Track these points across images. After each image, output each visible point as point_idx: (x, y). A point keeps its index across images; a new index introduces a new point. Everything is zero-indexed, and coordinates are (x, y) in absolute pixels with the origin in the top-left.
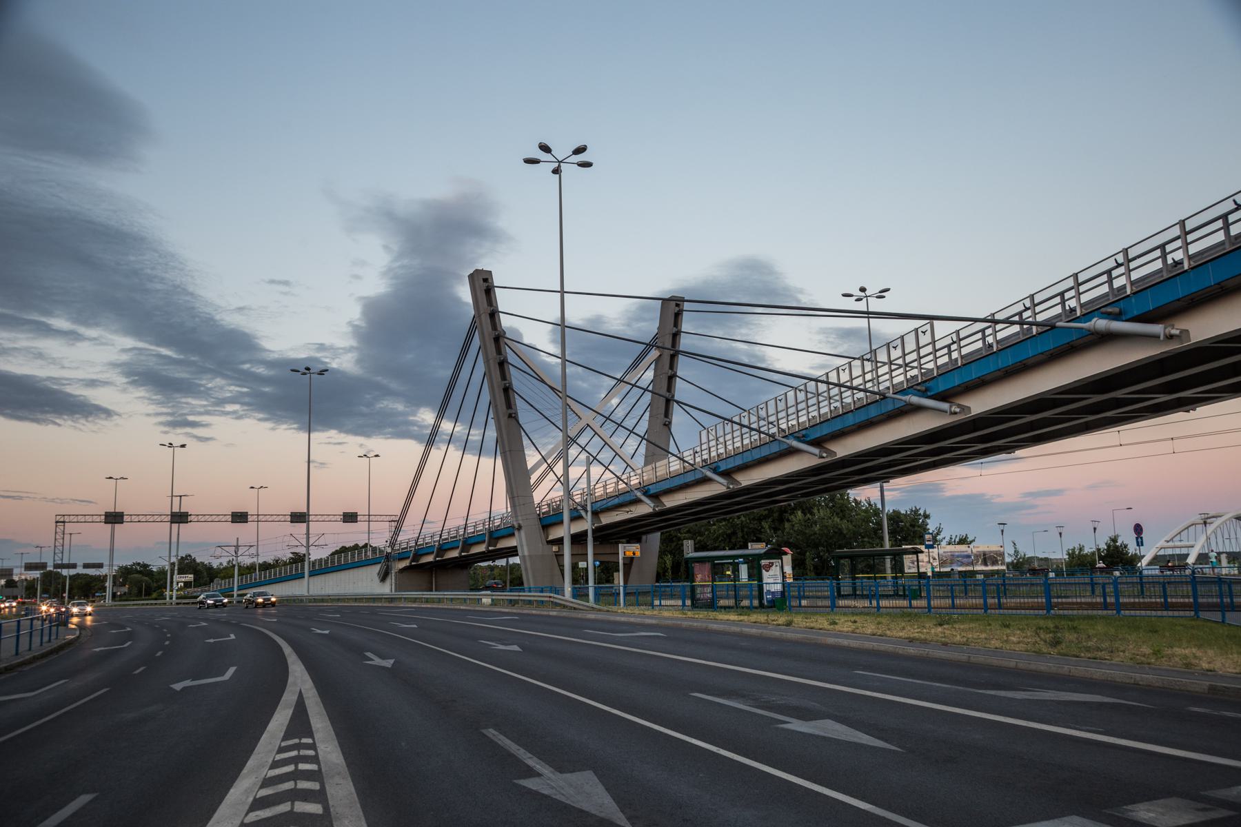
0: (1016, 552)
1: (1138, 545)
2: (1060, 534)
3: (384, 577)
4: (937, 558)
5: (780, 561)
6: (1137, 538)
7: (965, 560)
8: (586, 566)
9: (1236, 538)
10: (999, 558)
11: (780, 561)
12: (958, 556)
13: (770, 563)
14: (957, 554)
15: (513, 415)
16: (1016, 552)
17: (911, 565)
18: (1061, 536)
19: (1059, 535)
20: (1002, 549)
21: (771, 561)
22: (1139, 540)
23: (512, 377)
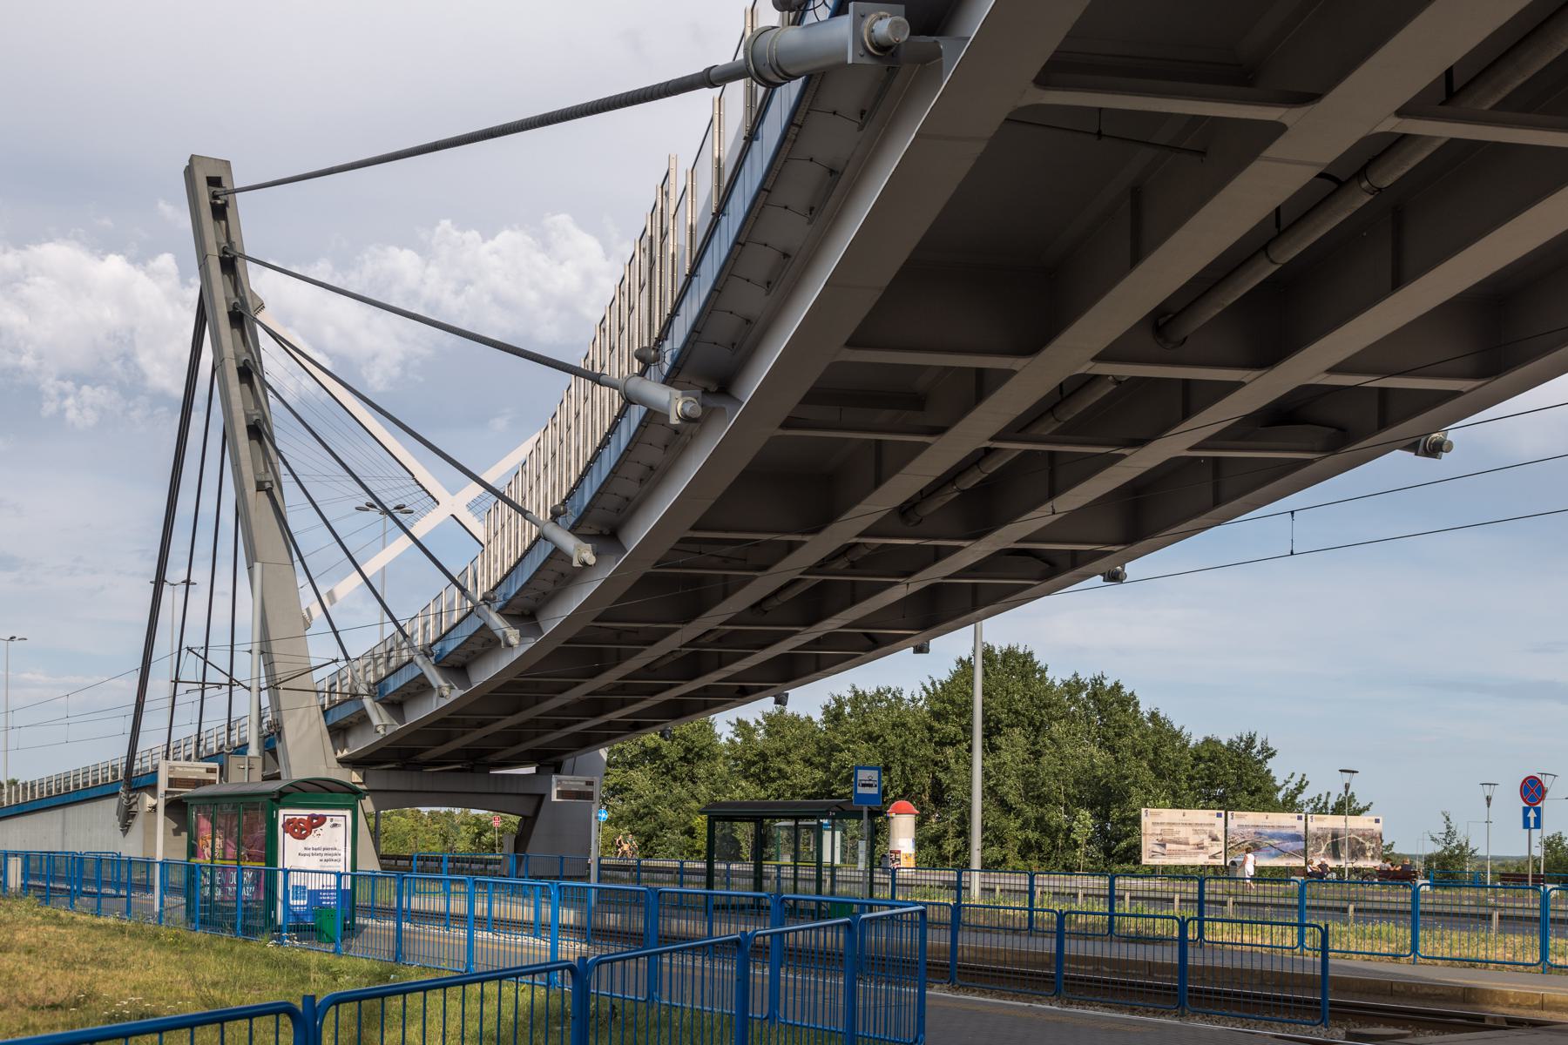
0: (1450, 833)
1: (1526, 825)
2: (1489, 799)
3: (127, 818)
4: (1221, 836)
5: (348, 813)
6: (1526, 811)
7: (1290, 845)
8: (1303, 847)
9: (188, 582)
10: (1368, 845)
11: (348, 813)
12: (1272, 837)
13: (312, 817)
14: (1269, 831)
15: (268, 485)
16: (1450, 833)
17: (1158, 849)
18: (1489, 805)
19: (1486, 802)
20: (589, 789)
21: (318, 812)
22: (1532, 814)
23: (603, 479)
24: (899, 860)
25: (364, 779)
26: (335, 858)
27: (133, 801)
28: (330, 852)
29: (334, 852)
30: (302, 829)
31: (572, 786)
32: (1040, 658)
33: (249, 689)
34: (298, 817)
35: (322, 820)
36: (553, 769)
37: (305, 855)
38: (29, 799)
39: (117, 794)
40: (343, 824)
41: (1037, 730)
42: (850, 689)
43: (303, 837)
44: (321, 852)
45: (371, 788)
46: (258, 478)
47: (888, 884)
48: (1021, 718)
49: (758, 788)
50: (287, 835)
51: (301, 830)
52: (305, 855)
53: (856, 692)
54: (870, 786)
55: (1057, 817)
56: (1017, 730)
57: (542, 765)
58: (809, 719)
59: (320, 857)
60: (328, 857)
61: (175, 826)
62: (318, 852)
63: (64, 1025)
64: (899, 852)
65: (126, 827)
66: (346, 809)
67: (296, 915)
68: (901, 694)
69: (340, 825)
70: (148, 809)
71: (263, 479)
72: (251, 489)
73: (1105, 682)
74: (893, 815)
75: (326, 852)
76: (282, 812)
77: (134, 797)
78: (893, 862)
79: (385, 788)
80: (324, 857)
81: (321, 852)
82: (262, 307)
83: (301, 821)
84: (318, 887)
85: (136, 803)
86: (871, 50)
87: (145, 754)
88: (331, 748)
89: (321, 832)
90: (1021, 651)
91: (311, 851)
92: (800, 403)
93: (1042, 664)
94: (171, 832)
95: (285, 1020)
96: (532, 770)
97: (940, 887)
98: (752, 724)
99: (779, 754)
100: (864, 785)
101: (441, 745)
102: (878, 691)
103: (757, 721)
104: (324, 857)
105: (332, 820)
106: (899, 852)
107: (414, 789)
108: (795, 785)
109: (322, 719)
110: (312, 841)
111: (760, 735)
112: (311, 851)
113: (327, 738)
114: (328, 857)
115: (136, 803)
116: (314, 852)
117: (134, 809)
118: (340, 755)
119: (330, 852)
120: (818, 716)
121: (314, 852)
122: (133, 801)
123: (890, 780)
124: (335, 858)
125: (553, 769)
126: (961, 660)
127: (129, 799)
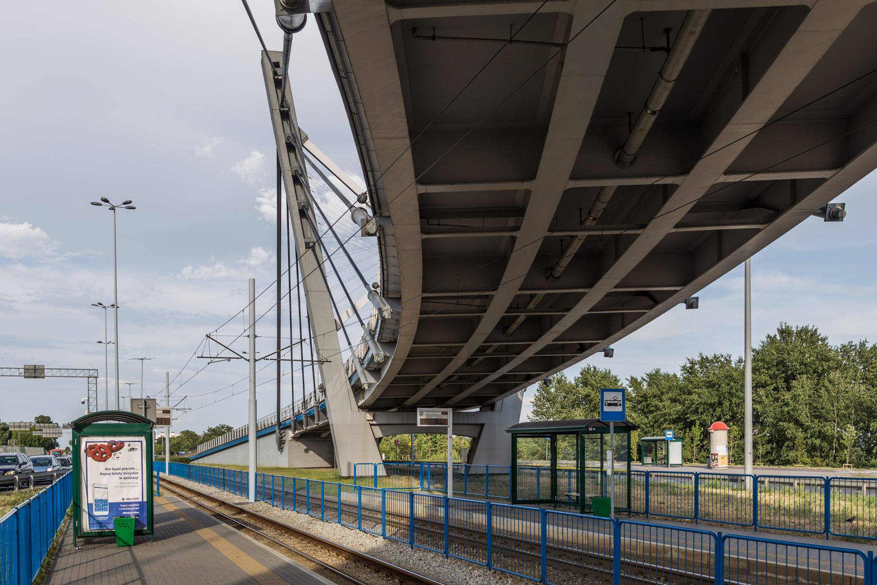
5: (143, 439)
11: (143, 439)
24: (717, 459)
25: (374, 417)
26: (132, 476)
27: (283, 434)
28: (129, 471)
29: (132, 471)
30: (103, 453)
31: (432, 415)
32: (822, 333)
33: (248, 360)
34: (99, 444)
35: (121, 445)
36: (490, 408)
37: (106, 474)
38: (244, 435)
39: (274, 432)
40: (139, 448)
41: (819, 376)
42: (699, 355)
43: (105, 460)
44: (121, 471)
45: (380, 422)
46: (306, 241)
47: (691, 478)
48: (808, 368)
49: (643, 417)
50: (90, 459)
51: (101, 454)
52: (106, 474)
53: (702, 358)
54: (616, 405)
55: (831, 429)
56: (805, 376)
57: (483, 406)
58: (675, 375)
59: (119, 476)
60: (127, 476)
61: (306, 447)
62: (117, 471)
63: (643, 491)
64: (717, 454)
65: (281, 449)
66: (141, 436)
67: (100, 524)
68: (730, 358)
69: (137, 449)
70: (290, 439)
71: (309, 241)
72: (302, 249)
73: (867, 345)
74: (713, 431)
75: (125, 471)
76: (84, 440)
77: (284, 432)
78: (713, 461)
79: (401, 423)
80: (123, 476)
81: (121, 471)
82: (307, 138)
83: (101, 447)
84: (118, 499)
85: (285, 435)
86: (831, 214)
87: (287, 408)
88: (354, 400)
89: (120, 456)
90: (810, 328)
91: (112, 471)
92: (688, 212)
93: (823, 336)
94: (304, 451)
95: (751, 477)
96: (478, 409)
97: (724, 480)
98: (639, 380)
99: (655, 397)
100: (609, 405)
101: (413, 395)
102: (715, 356)
103: (642, 378)
104: (123, 476)
105: (129, 445)
106: (717, 454)
107: (404, 423)
108: (665, 413)
109: (348, 382)
110: (113, 462)
111: (645, 386)
112: (112, 471)
113: (352, 394)
114: (127, 476)
115: (285, 435)
116: (114, 471)
117: (284, 439)
118: (361, 403)
119: (129, 471)
120: (679, 374)
121: (114, 471)
122: (283, 434)
123: (722, 411)
124: (132, 476)
125: (490, 408)
126: (769, 336)
127: (281, 434)
